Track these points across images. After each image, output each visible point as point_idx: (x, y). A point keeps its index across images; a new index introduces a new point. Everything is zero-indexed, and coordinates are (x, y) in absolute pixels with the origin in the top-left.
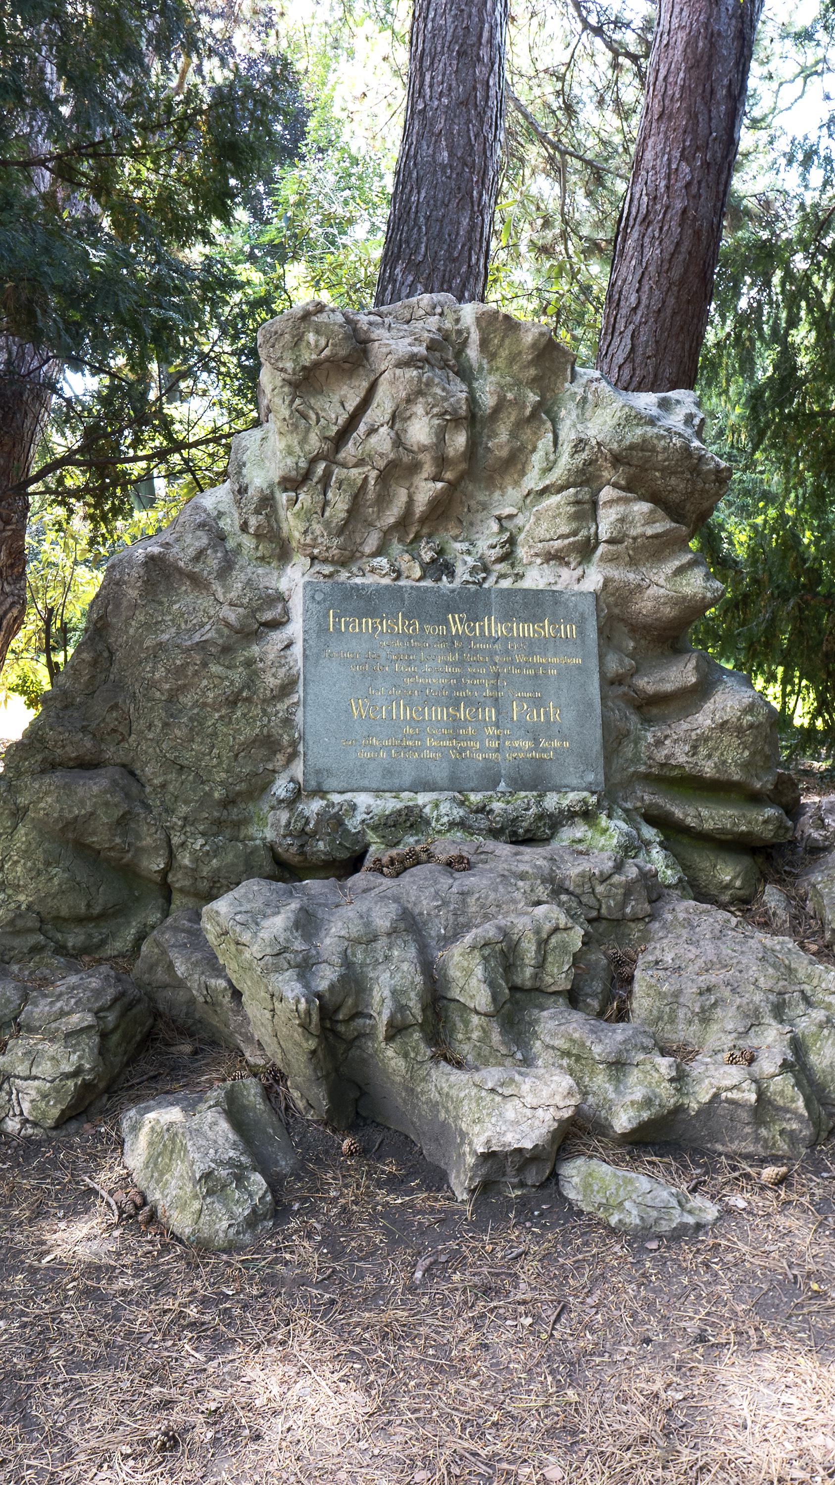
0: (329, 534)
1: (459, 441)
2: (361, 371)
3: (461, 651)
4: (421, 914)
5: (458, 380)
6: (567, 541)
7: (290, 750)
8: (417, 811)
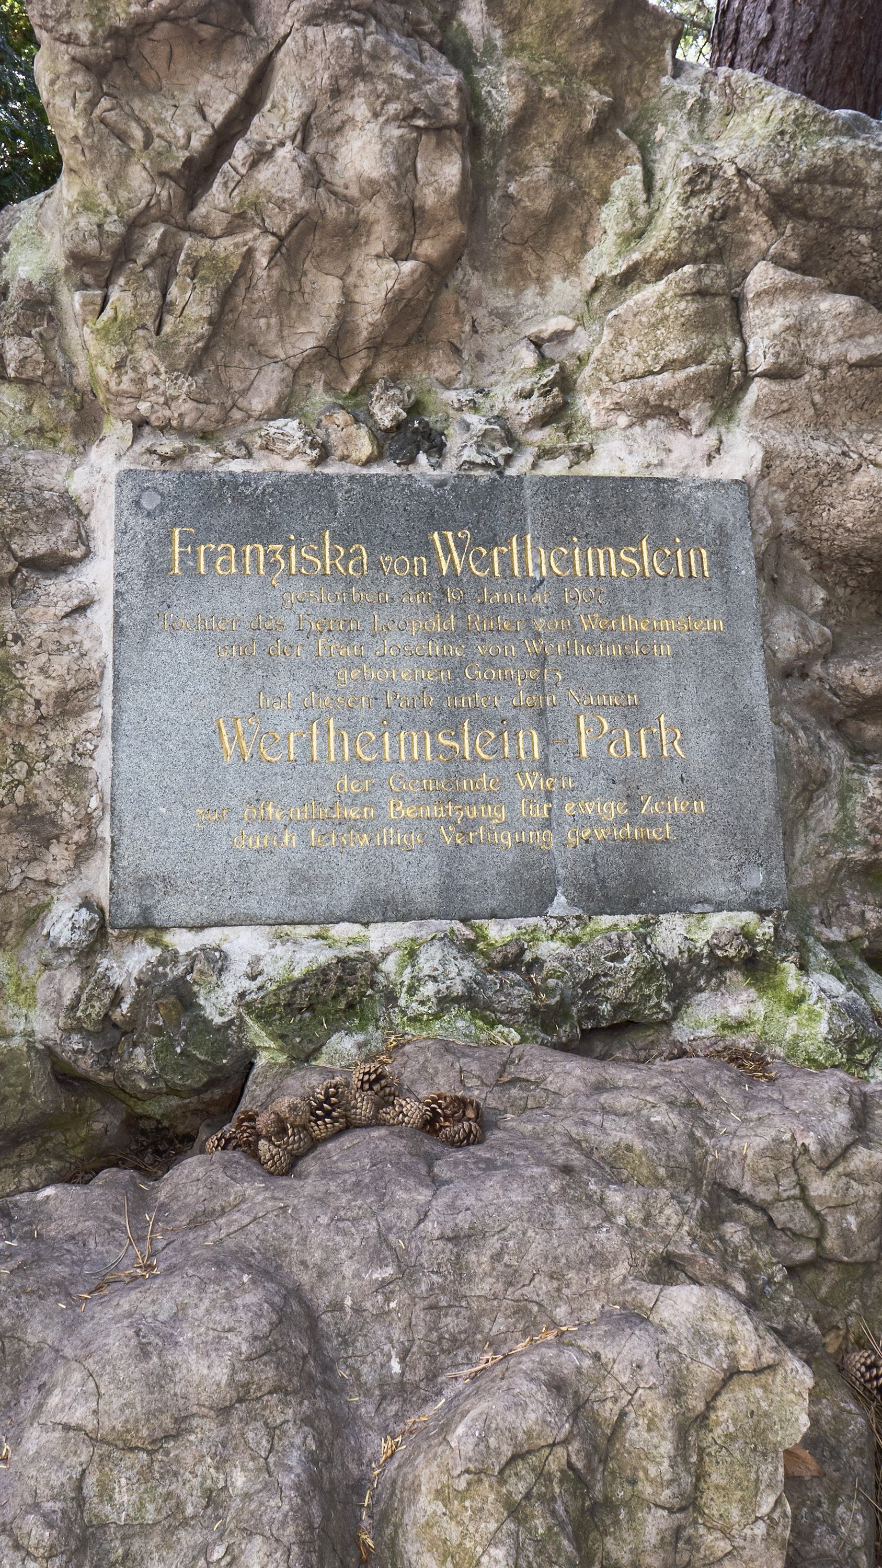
0: (171, 369)
1: (446, 172)
2: (239, 43)
3: (461, 607)
4: (336, 1306)
5: (442, 60)
6: (681, 375)
7: (79, 836)
8: (363, 969)
